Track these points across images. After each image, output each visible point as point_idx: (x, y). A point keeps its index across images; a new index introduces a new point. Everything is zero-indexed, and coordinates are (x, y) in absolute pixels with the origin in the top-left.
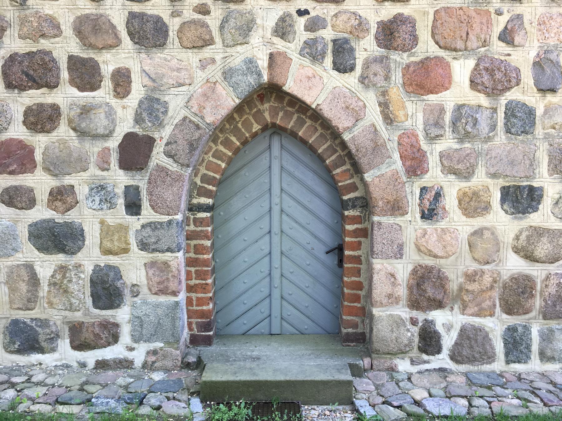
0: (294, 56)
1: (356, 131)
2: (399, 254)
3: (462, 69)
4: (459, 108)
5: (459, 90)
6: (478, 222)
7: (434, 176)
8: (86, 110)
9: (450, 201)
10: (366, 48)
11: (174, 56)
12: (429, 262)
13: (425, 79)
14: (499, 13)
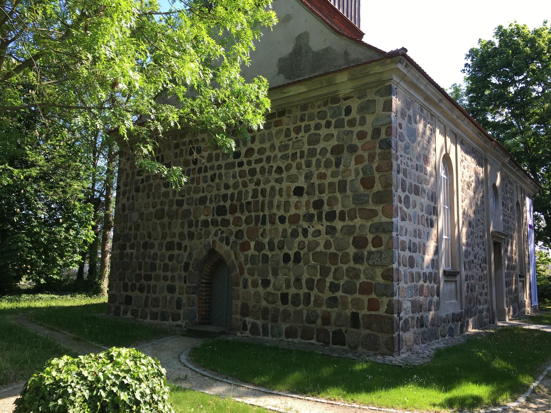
0: (217, 241)
1: (229, 261)
2: (238, 299)
3: (252, 244)
4: (252, 255)
5: (252, 251)
6: (256, 290)
7: (246, 275)
8: (179, 255)
9: (249, 283)
10: (232, 238)
11: (195, 241)
12: (245, 301)
13: (245, 247)
14: (260, 228)
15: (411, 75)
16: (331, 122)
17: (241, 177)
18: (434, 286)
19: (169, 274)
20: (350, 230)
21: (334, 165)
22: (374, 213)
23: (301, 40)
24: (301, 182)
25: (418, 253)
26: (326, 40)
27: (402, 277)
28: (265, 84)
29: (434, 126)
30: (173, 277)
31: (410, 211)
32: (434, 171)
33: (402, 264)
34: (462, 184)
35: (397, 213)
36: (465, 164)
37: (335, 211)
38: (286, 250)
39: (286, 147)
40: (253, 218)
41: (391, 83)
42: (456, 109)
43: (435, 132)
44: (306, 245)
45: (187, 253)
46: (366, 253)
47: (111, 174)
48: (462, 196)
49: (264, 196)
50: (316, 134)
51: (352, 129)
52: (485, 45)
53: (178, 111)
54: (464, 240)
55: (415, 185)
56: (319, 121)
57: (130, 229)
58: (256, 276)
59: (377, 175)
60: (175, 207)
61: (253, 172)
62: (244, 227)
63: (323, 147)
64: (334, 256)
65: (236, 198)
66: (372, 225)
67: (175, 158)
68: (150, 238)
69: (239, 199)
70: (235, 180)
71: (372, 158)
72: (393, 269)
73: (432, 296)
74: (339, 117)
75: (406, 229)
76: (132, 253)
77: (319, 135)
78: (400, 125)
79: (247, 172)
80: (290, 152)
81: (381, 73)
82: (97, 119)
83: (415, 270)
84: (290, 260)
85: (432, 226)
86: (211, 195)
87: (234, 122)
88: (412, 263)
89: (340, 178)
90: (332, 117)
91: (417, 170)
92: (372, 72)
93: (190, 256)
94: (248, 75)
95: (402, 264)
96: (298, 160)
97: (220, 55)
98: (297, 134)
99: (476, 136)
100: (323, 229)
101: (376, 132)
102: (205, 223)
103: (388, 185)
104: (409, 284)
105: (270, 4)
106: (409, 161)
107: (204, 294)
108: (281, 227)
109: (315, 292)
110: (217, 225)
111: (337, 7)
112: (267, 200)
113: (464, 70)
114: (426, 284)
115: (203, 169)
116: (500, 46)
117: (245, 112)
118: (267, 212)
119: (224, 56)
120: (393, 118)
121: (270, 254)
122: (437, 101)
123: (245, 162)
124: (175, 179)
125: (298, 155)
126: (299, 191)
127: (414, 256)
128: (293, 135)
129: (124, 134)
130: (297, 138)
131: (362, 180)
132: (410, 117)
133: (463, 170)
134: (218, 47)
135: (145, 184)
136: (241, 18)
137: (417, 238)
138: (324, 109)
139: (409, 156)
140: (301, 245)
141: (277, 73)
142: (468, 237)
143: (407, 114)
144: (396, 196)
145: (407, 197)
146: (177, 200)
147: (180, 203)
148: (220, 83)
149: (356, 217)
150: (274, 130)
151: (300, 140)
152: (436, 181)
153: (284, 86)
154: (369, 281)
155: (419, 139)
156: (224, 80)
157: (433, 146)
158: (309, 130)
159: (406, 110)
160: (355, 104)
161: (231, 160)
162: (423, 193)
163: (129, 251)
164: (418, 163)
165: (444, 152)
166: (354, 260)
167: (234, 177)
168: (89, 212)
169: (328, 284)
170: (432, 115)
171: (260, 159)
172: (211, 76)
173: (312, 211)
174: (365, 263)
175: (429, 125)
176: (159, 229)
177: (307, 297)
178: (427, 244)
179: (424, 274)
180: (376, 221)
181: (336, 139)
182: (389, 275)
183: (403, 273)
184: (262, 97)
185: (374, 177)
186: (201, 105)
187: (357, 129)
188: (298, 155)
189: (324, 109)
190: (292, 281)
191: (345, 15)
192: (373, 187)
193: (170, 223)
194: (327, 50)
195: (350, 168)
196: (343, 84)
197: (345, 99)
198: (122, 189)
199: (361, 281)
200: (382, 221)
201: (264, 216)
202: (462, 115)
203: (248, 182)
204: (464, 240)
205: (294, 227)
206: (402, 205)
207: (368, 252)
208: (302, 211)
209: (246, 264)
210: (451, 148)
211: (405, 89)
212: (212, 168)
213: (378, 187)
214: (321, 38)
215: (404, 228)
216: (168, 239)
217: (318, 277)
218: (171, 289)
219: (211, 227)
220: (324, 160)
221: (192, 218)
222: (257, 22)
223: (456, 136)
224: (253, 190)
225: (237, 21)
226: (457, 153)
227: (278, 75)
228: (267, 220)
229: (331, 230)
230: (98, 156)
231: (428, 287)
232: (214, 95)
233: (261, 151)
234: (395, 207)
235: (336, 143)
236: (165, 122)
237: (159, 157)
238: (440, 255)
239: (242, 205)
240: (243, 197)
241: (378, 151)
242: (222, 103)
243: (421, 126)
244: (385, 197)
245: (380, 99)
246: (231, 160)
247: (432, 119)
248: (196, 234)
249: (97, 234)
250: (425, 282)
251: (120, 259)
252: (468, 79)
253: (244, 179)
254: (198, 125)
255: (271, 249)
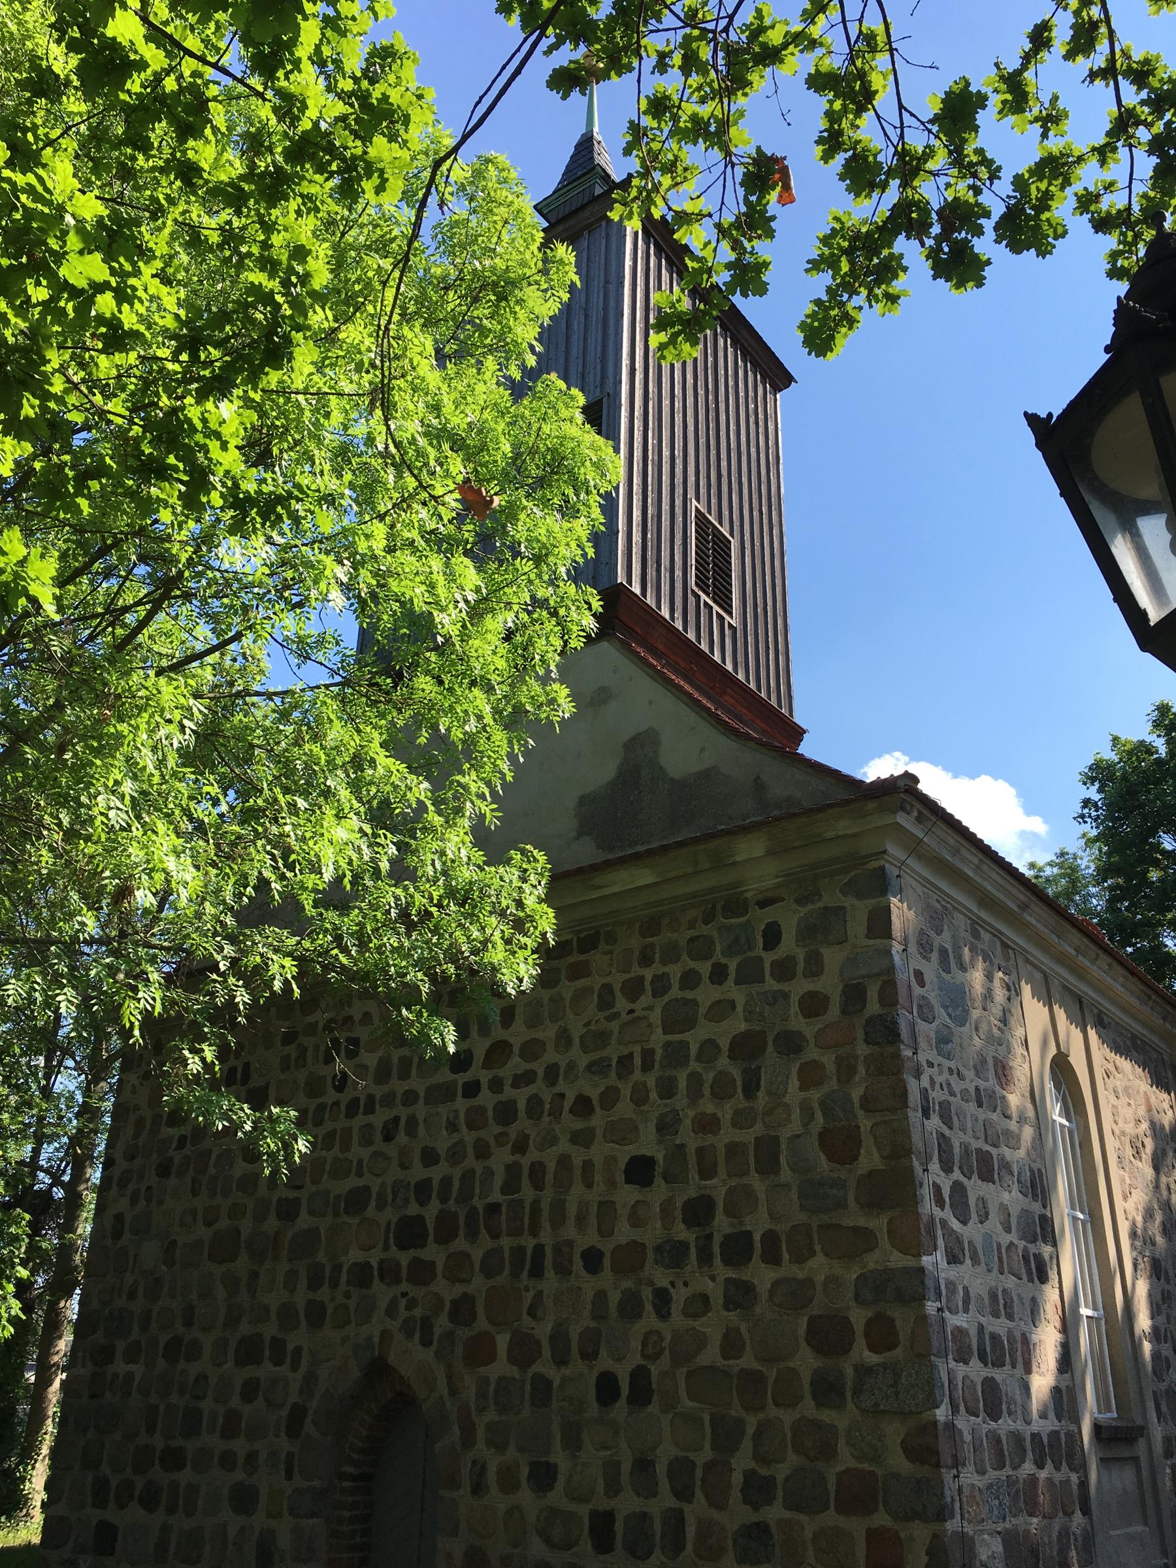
3: (502, 1341)
4: (501, 1379)
5: (501, 1367)
9: (492, 1476)
10: (442, 1323)
13: (480, 1352)
14: (527, 1289)
15: (936, 841)
16: (726, 966)
17: (471, 1126)
18: (1068, 1481)
19: (240, 1446)
20: (796, 1295)
21: (739, 1090)
22: (864, 1240)
23: (639, 753)
24: (648, 1144)
25: (1008, 1367)
26: (703, 750)
27: (968, 1451)
28: (539, 866)
29: (1014, 976)
30: (251, 1457)
31: (971, 1232)
32: (1030, 1106)
33: (962, 1408)
34: (1118, 1145)
35: (935, 1238)
36: (1118, 1082)
37: (749, 1234)
38: (605, 1362)
39: (602, 1039)
40: (507, 1255)
41: (882, 863)
42: (1069, 927)
43: (1018, 993)
44: (666, 1343)
45: (300, 1375)
46: (849, 1371)
47: (90, 1120)
48: (1123, 1180)
49: (538, 1186)
50: (686, 1002)
51: (784, 987)
52: (1130, 753)
53: (299, 943)
54: (1144, 1322)
55: (979, 1151)
56: (692, 964)
57: (132, 1296)
58: (512, 1453)
59: (865, 1123)
60: (272, 1223)
61: (506, 1113)
62: (478, 1285)
63: (706, 1037)
64: (752, 1382)
65: (454, 1194)
66: (862, 1278)
67: (283, 1071)
68: (188, 1323)
69: (465, 1196)
70: (455, 1137)
71: (846, 1070)
72: (935, 1423)
73: (1069, 1514)
74: (749, 954)
75: (965, 1289)
76: (130, 1376)
77: (694, 1003)
78: (919, 975)
79: (490, 1113)
80: (613, 1052)
81: (853, 836)
82: (63, 986)
83: (1006, 1425)
84: (618, 1396)
85: (1043, 1278)
86: (383, 1184)
87: (452, 970)
88: (993, 1401)
89: (758, 1129)
90: (729, 951)
91: (980, 1105)
92: (830, 834)
93: (310, 1380)
94: (493, 845)
95: (962, 1408)
96: (637, 1075)
97: (419, 802)
98: (633, 1002)
99: (1137, 1003)
100: (715, 1290)
101: (854, 995)
102: (362, 1275)
103: (899, 1150)
104: (992, 1475)
105: (553, 667)
106: (954, 1080)
107: (346, 1514)
108: (588, 1285)
109: (696, 1510)
110: (397, 1281)
111: (729, 667)
112: (547, 1197)
113: (1082, 816)
114: (1043, 1475)
115: (362, 1102)
116: (1170, 753)
117: (485, 942)
118: (546, 1237)
119: (428, 803)
120: (897, 958)
121: (555, 1375)
122: (1015, 908)
123: (484, 1082)
124: (271, 1144)
125: (638, 1061)
126: (640, 1171)
127: (998, 1378)
128: (621, 1004)
129: (132, 1024)
130: (631, 1011)
131: (823, 1136)
132: (943, 952)
133: (1113, 1100)
134: (412, 779)
135: (188, 1150)
136: (478, 702)
137: (1003, 1319)
138: (705, 930)
139: (952, 1064)
140: (652, 1346)
141: (574, 834)
142: (1155, 1311)
143: (936, 945)
144: (926, 1186)
145: (958, 1188)
146: (280, 1199)
147: (288, 1210)
148: (415, 868)
149: (813, 1253)
150: (567, 989)
151: (639, 1018)
152: (1039, 1137)
153: (595, 868)
154: (865, 1466)
155: (976, 1014)
156: (428, 862)
157: (1019, 1032)
158: (666, 989)
159: (932, 934)
160: (790, 918)
161: (445, 1075)
162: (1003, 1172)
163: (120, 1367)
164: (982, 1084)
165: (1052, 1051)
166: (815, 1397)
167: (452, 1127)
168: (16, 1239)
169: (737, 1479)
170: (1005, 946)
171: (527, 1072)
172: (393, 850)
173: (682, 1233)
174: (850, 1405)
175: (1000, 974)
176: (221, 1293)
177: (675, 1521)
178: (1035, 1338)
179: (1035, 1437)
180: (871, 1266)
181: (741, 1015)
182: (928, 1447)
183: (968, 1437)
184: (530, 902)
185: (858, 1127)
186: (362, 926)
187: (799, 987)
188: (638, 1061)
189: (705, 930)
190: (626, 1468)
191: (752, 686)
192: (856, 1158)
193: (254, 1275)
194: (707, 776)
195: (787, 1099)
196: (755, 863)
197: (762, 904)
198: (121, 1165)
199: (840, 1468)
200: (891, 1265)
201: (539, 1250)
202: (1091, 946)
203: (492, 1142)
204: (1144, 1322)
205: (628, 1284)
206: (947, 1214)
207: (856, 1371)
208: (652, 1234)
209: (482, 1410)
210: (1073, 1038)
211: (924, 879)
212: (389, 1100)
213: (870, 1159)
214: (689, 746)
215: (957, 1287)
216: (245, 1328)
217: (706, 1454)
218: (244, 1500)
219: (377, 1286)
220: (711, 1075)
221: (321, 1257)
222: (519, 710)
223: (1080, 1002)
224: (508, 1167)
225: (466, 711)
226: (1087, 1049)
227: (577, 838)
228: (548, 1262)
229: (740, 1295)
230: (60, 1063)
231: (1049, 1481)
232: (397, 898)
233: (531, 1050)
234: (925, 1219)
235: (743, 1027)
236: (255, 978)
237: (235, 1076)
238: (1077, 1374)
239: (472, 1214)
240: (477, 1191)
241: (862, 1050)
242: (421, 921)
243: (977, 977)
244: (893, 1189)
245: (857, 903)
246: (445, 1075)
247: (1006, 957)
248: (330, 1311)
249: (27, 1308)
250: (1041, 1466)
251: (93, 1396)
252: (1097, 839)
253: (482, 1134)
254: (352, 980)
255: (561, 1360)
